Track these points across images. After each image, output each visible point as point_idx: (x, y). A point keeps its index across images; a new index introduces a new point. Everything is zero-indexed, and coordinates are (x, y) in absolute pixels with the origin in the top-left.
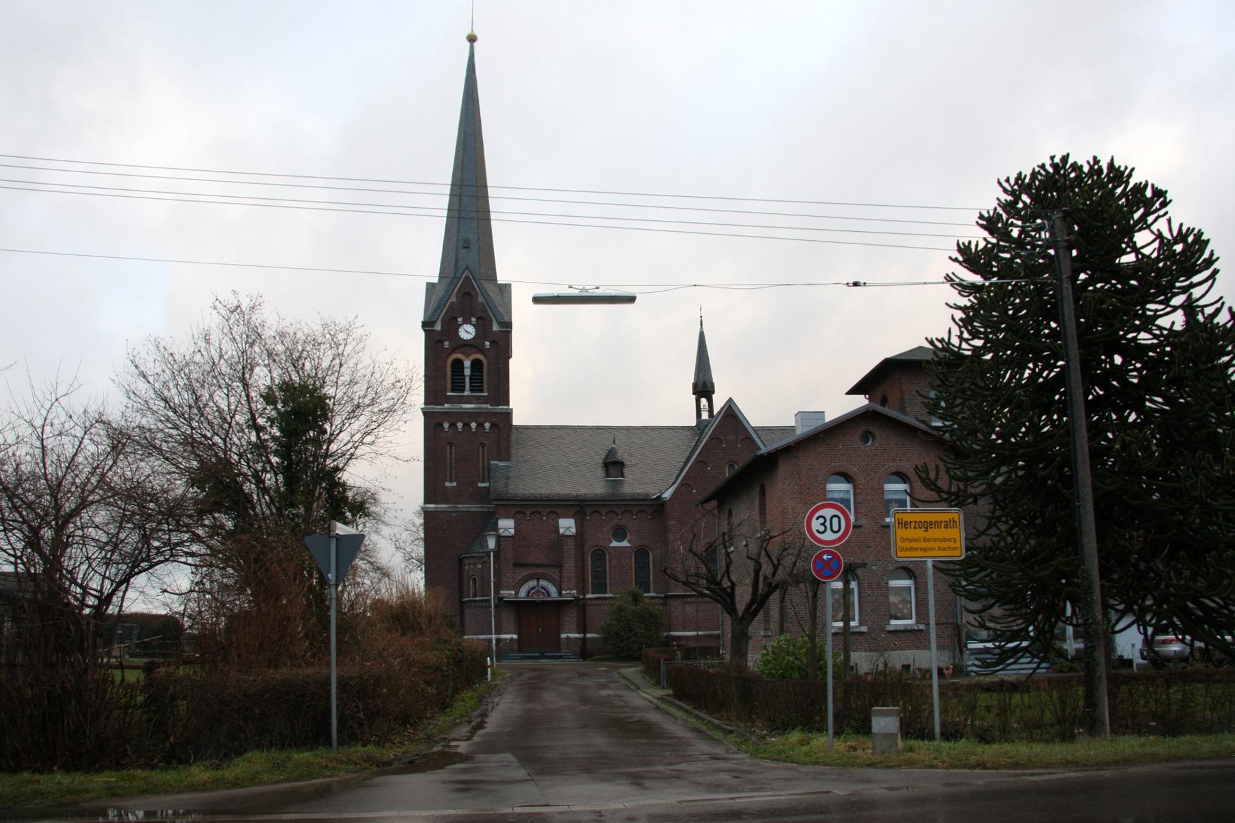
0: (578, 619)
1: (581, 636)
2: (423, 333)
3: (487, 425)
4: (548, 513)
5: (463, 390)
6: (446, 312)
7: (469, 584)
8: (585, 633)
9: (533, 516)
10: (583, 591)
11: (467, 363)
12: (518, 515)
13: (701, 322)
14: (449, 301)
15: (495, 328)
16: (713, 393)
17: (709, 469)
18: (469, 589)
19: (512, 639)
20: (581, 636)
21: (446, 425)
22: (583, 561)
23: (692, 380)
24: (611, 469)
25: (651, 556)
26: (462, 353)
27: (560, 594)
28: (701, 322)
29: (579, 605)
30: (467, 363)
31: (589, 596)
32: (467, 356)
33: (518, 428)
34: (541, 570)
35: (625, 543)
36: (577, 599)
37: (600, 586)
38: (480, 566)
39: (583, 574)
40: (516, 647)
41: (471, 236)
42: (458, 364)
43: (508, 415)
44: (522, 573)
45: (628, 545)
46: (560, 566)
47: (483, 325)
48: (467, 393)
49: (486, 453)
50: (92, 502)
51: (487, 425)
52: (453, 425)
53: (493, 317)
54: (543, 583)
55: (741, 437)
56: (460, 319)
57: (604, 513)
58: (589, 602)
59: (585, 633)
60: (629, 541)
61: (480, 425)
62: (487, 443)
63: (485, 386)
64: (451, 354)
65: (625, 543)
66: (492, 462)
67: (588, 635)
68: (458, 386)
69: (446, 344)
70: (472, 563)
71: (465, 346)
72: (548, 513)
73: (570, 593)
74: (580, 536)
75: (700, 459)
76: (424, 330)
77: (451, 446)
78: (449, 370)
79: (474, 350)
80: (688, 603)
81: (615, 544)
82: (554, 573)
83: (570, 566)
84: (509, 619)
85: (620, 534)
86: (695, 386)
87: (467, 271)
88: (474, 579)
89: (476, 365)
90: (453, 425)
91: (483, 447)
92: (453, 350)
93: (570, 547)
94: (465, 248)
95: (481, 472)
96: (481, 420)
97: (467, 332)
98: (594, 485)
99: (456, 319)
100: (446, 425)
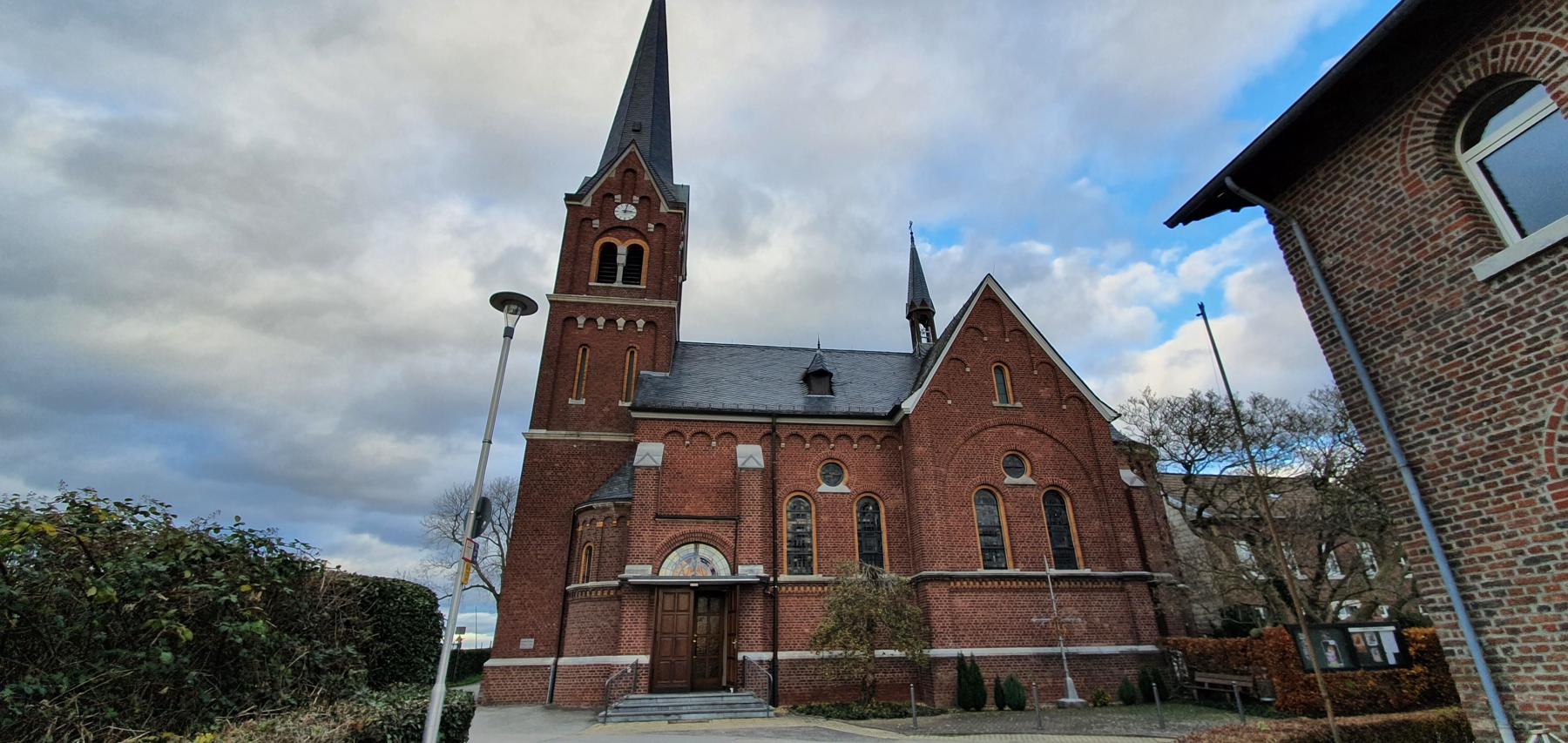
0: (764, 622)
1: (768, 656)
2: (565, 211)
3: (641, 323)
4: (720, 436)
5: (613, 280)
6: (601, 187)
7: (580, 555)
8: (775, 649)
9: (695, 440)
10: (774, 568)
11: (622, 250)
12: (670, 438)
13: (912, 238)
14: (606, 176)
15: (664, 208)
16: (934, 313)
17: (968, 370)
18: (578, 569)
19: (636, 666)
20: (768, 656)
21: (581, 320)
22: (774, 515)
23: (905, 300)
24: (813, 381)
25: (882, 510)
26: (617, 237)
27: (734, 572)
28: (912, 238)
29: (767, 590)
30: (622, 250)
31: (783, 578)
32: (623, 240)
33: (685, 344)
34: (703, 527)
35: (842, 488)
36: (763, 582)
37: (802, 561)
38: (600, 524)
39: (775, 537)
40: (644, 682)
41: (643, 121)
42: (609, 252)
43: (673, 316)
44: (670, 532)
45: (847, 490)
46: (736, 519)
47: (647, 203)
48: (618, 284)
49: (635, 359)
50: (1113, 706)
51: (641, 323)
52: (591, 320)
53: (661, 197)
54: (704, 550)
55: (1008, 329)
56: (618, 197)
57: (808, 438)
58: (784, 588)
59: (775, 649)
60: (847, 485)
61: (631, 322)
62: (638, 347)
63: (644, 277)
64: (600, 236)
65: (842, 488)
66: (642, 372)
67: (782, 655)
68: (606, 273)
69: (596, 223)
70: (589, 518)
71: (622, 228)
72: (720, 436)
73: (752, 571)
74: (770, 476)
75: (954, 356)
76: (568, 206)
77: (585, 350)
78: (596, 256)
79: (633, 234)
80: (957, 590)
81: (824, 488)
82: (724, 532)
83: (753, 520)
84: (635, 622)
85: (833, 471)
86: (911, 305)
87: (633, 146)
88: (590, 548)
89: (635, 252)
90: (591, 320)
91: (632, 353)
92: (605, 232)
93: (753, 491)
94: (634, 131)
95: (625, 386)
96: (633, 315)
97: (625, 212)
98: (792, 398)
99: (612, 196)
100: (581, 320)
